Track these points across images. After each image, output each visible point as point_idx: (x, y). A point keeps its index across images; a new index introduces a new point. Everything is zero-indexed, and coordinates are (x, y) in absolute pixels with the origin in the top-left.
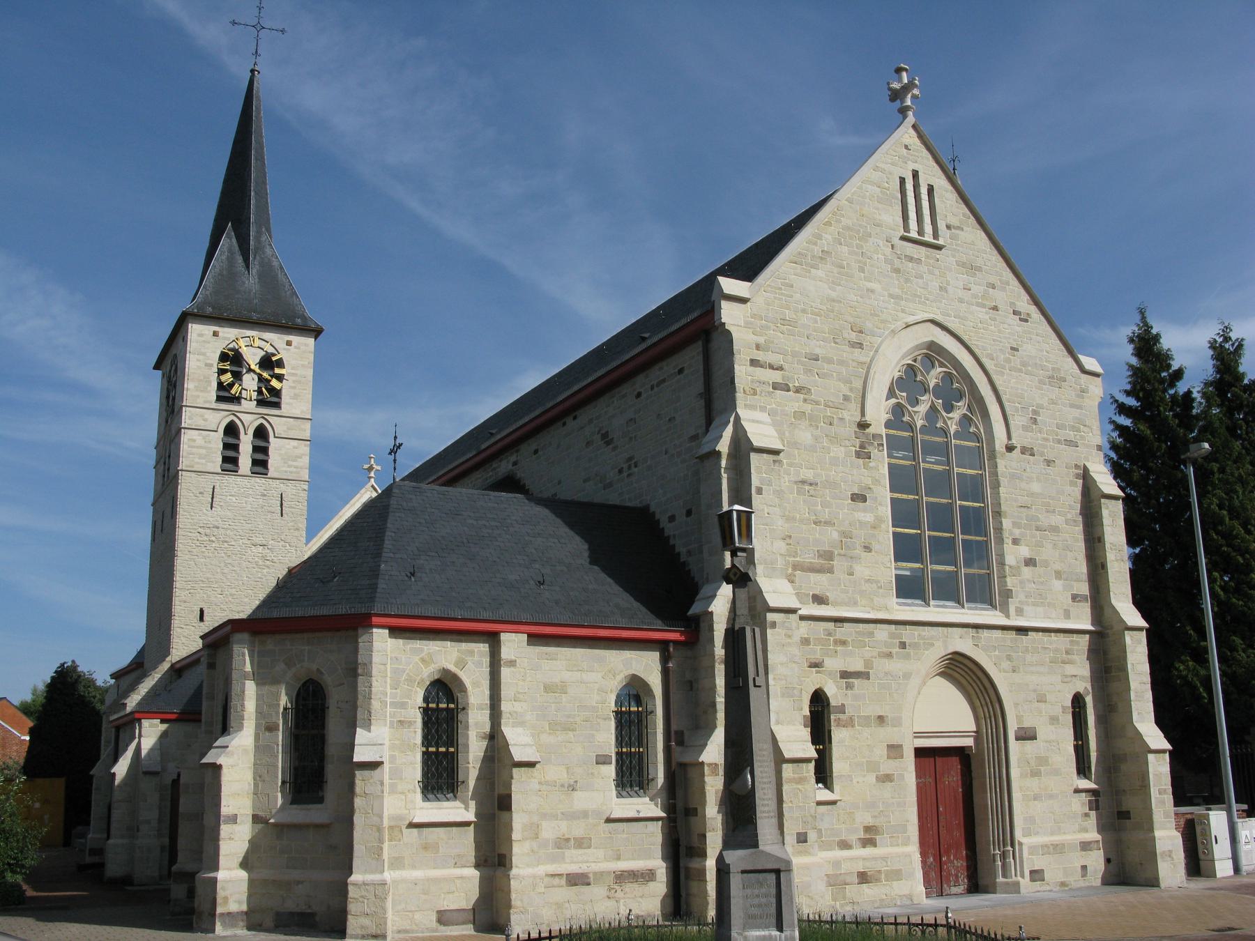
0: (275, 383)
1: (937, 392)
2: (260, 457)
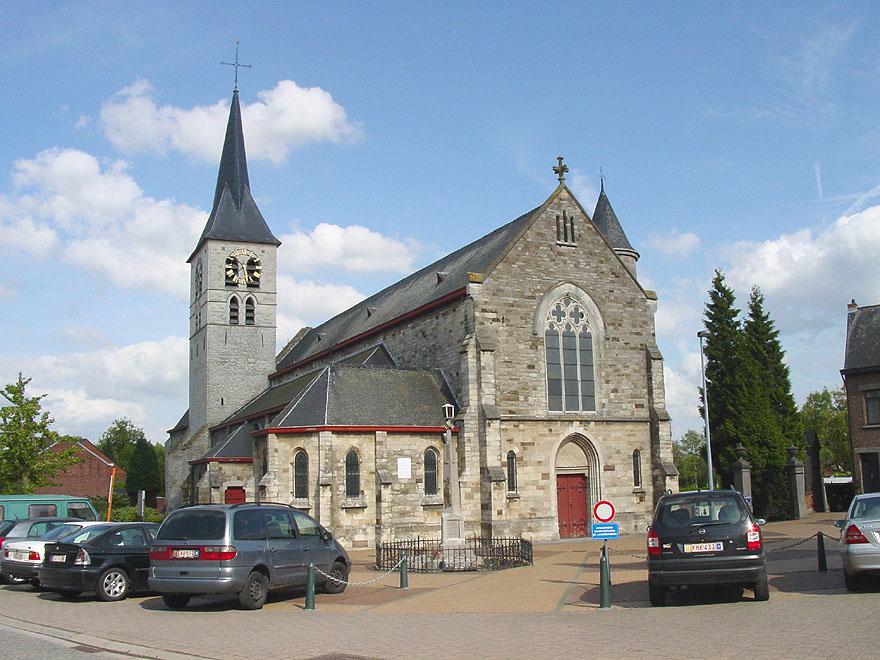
0: (256, 274)
1: (571, 315)
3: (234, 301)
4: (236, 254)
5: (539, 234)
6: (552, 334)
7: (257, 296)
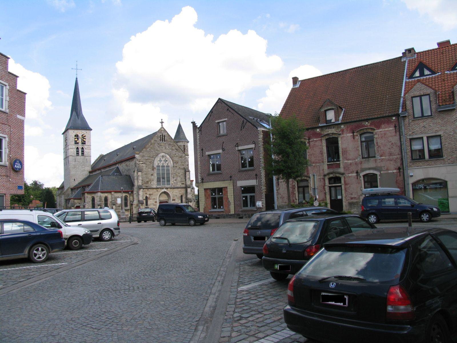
1: (162, 161)
2: (82, 153)
3: (77, 148)
4: (78, 133)
5: (155, 140)
6: (158, 166)
7: (85, 147)
